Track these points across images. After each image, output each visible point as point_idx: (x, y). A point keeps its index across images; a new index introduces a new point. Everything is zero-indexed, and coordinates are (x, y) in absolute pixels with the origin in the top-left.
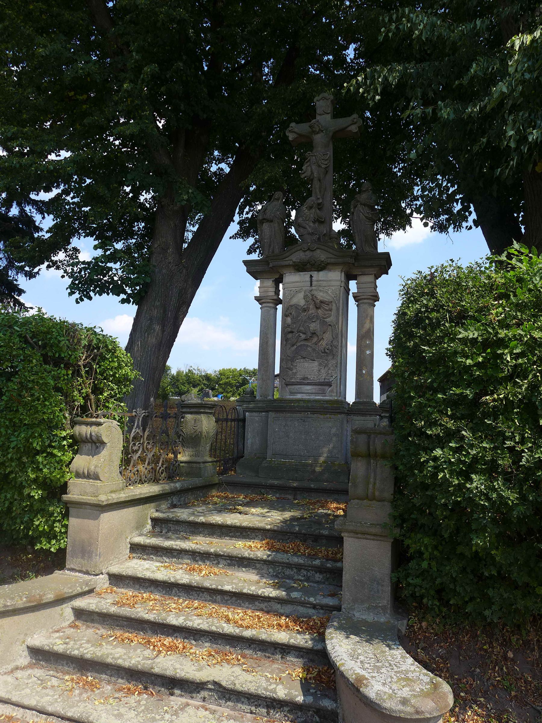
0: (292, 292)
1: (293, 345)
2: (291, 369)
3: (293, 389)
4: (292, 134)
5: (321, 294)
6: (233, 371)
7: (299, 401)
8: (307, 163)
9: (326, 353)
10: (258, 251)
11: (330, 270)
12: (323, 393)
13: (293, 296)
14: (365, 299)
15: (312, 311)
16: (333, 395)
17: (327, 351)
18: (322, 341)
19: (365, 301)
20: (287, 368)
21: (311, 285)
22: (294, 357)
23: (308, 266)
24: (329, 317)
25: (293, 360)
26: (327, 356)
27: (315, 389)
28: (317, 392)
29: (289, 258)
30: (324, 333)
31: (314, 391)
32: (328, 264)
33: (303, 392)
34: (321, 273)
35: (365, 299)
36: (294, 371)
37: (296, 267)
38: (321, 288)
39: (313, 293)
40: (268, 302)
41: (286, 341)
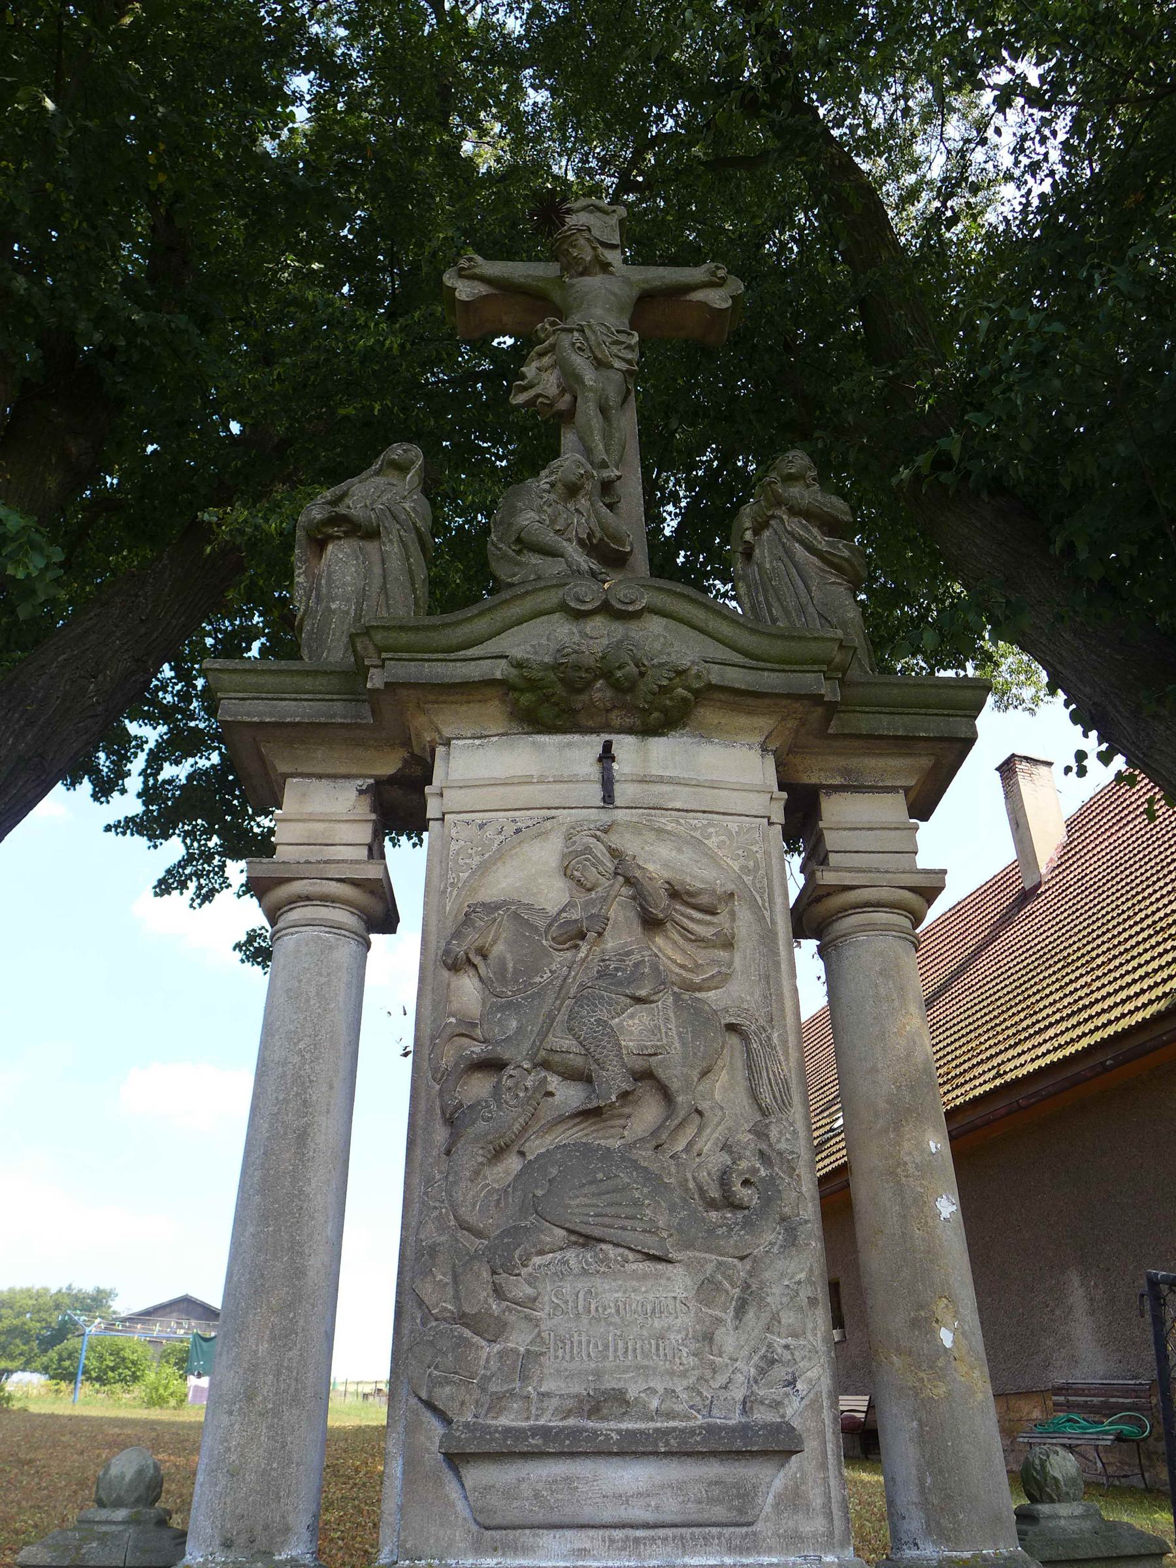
0: (489, 832)
1: (499, 1153)
2: (493, 1329)
3: (510, 1494)
4: (467, 282)
5: (665, 851)
6: (39, 1295)
8: (541, 355)
9: (737, 1207)
10: (192, 885)
11: (706, 734)
13: (500, 856)
14: (878, 905)
15: (622, 935)
16: (807, 1528)
17: (743, 1194)
18: (690, 1131)
19: (882, 917)
20: (462, 1319)
21: (608, 798)
22: (514, 1232)
23: (600, 692)
24: (723, 979)
25: (503, 1255)
26: (747, 1224)
27: (679, 1488)
28: (693, 1511)
29: (491, 647)
30: (704, 1074)
31: (671, 1508)
32: (709, 693)
33: (588, 1513)
34: (659, 746)
35: (878, 905)
36: (519, 1340)
37: (526, 699)
38: (664, 821)
39: (615, 840)
40: (327, 900)
41: (450, 1122)
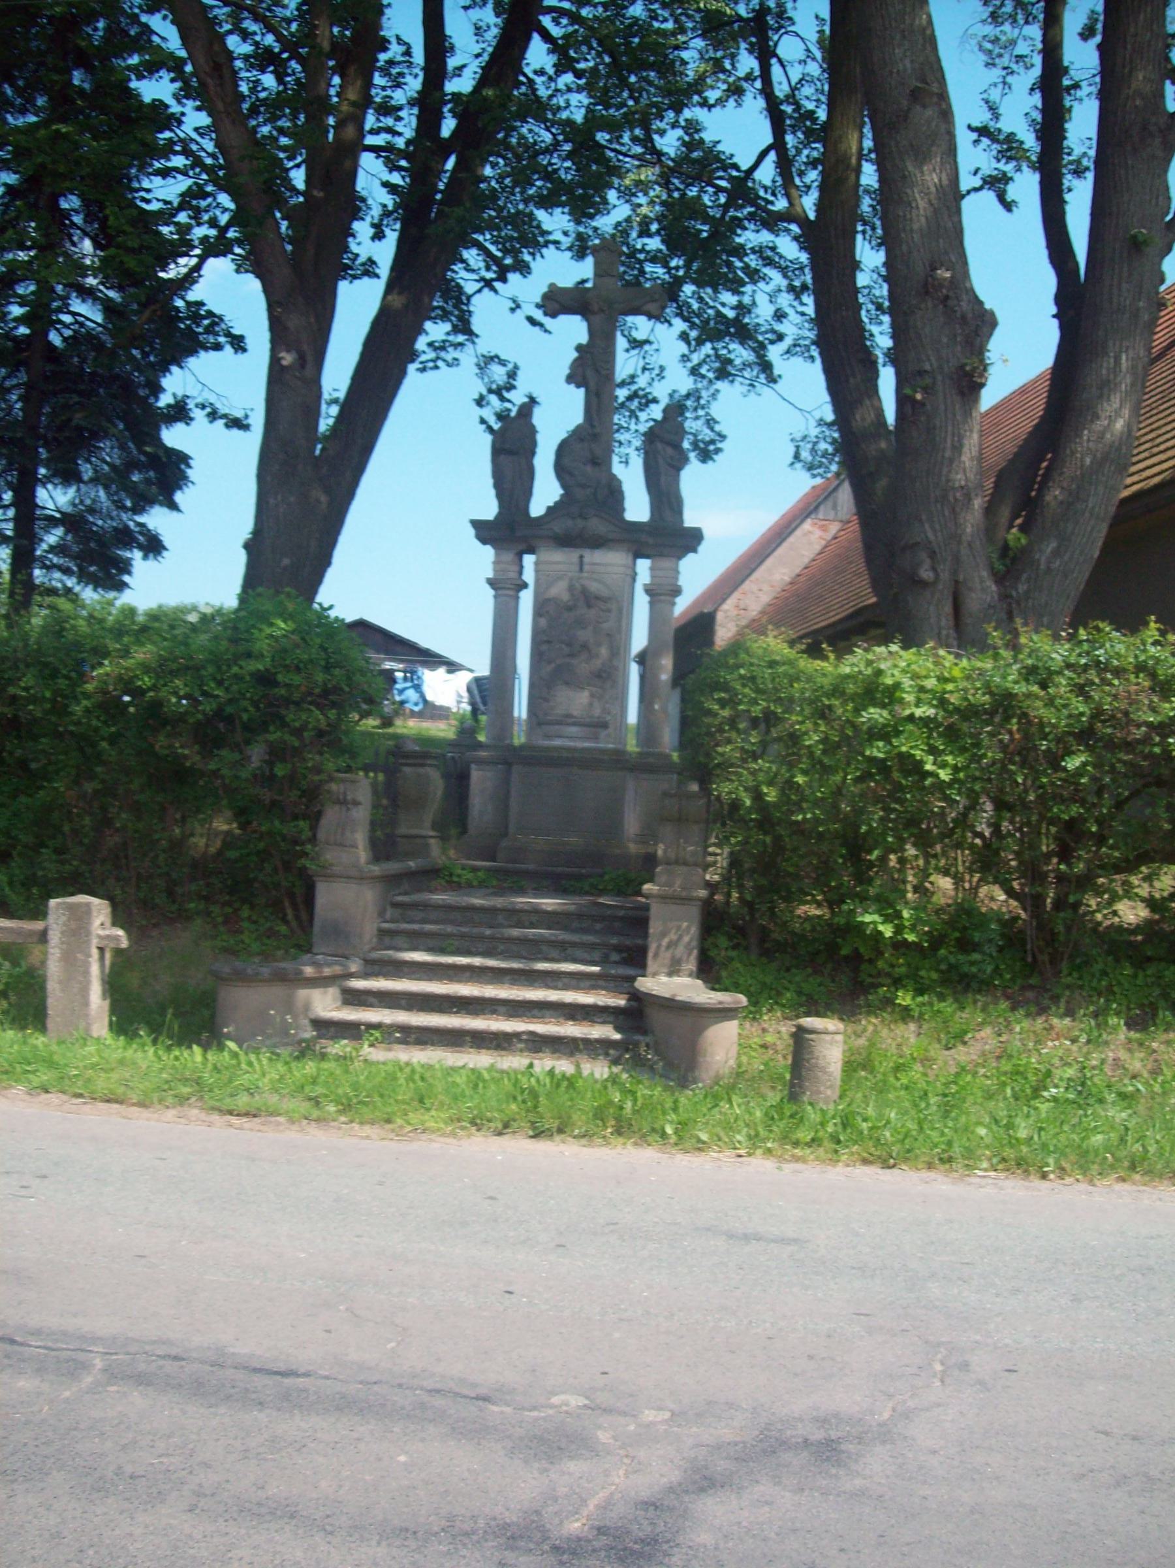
7: (557, 749)
12: (596, 738)
21: (581, 570)
